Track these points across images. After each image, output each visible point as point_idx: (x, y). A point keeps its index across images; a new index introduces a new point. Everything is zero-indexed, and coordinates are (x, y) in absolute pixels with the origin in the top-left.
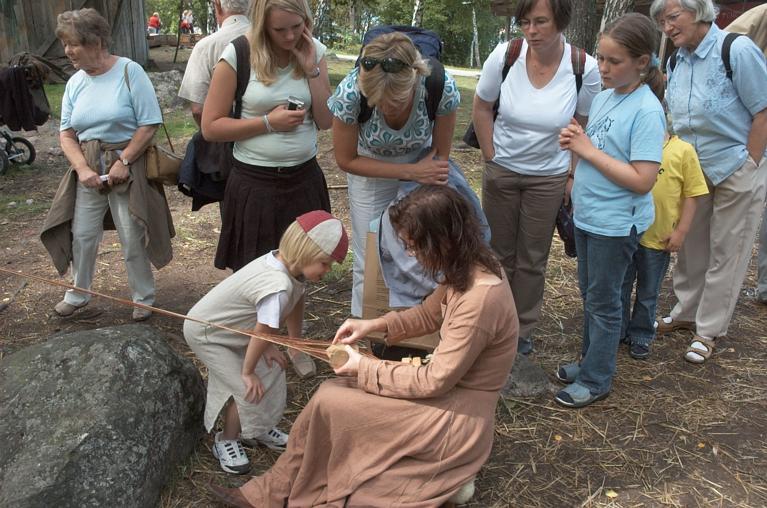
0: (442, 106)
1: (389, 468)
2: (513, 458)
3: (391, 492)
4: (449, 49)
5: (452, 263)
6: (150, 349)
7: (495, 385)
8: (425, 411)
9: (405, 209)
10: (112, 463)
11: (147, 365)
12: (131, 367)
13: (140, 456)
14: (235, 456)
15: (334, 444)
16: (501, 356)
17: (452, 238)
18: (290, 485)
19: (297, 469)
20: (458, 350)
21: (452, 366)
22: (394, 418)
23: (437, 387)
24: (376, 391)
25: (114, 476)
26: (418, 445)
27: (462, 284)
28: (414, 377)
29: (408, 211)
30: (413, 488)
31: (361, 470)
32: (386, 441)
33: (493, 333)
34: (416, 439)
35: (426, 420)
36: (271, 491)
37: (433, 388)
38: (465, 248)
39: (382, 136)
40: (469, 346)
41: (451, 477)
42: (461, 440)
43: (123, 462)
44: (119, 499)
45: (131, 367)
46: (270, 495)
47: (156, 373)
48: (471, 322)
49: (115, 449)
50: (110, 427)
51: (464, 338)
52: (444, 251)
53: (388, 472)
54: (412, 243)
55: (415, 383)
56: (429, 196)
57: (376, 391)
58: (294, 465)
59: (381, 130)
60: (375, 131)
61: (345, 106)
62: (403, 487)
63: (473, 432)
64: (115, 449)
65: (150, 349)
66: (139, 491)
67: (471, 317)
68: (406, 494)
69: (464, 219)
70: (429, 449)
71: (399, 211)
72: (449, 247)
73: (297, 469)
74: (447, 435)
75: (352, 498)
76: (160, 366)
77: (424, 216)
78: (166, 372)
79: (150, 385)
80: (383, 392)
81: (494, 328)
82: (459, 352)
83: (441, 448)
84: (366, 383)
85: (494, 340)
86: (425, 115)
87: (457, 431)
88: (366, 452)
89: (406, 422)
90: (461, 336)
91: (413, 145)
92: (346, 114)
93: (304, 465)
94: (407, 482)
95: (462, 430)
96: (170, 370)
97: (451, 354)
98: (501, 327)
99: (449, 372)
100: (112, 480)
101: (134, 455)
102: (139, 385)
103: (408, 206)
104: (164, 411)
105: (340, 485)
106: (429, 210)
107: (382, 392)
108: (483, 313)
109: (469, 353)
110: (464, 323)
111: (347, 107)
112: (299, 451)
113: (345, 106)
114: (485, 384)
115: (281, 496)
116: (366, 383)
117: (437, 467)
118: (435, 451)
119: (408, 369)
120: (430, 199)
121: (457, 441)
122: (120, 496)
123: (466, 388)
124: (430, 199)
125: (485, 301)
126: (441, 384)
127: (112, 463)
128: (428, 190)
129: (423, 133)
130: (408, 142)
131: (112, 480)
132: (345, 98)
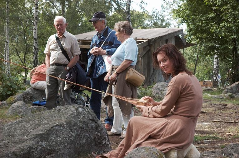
10: (63, 135)
42: (171, 132)
44: (62, 145)
49: (65, 131)
64: (65, 131)
65: (87, 110)
70: (159, 134)
73: (121, 149)
89: (154, 125)
114: (181, 113)
118: (160, 135)
122: (62, 144)
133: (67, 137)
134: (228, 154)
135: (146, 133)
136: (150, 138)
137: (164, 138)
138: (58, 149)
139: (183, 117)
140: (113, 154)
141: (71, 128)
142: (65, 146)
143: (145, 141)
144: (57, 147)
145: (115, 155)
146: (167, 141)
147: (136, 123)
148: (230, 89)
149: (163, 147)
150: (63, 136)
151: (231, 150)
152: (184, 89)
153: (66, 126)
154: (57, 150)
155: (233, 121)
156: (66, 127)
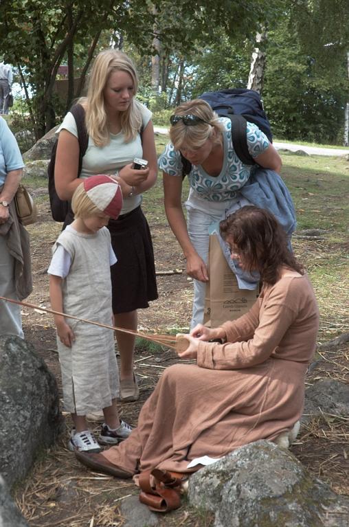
0: (252, 151)
1: (222, 419)
2: (329, 451)
3: (223, 440)
4: (310, 118)
5: (265, 261)
6: (25, 347)
7: (302, 358)
8: (248, 377)
9: (233, 221)
10: (6, 420)
11: (25, 358)
12: (13, 357)
13: (26, 418)
14: (90, 443)
15: (178, 410)
16: (307, 332)
17: (265, 243)
18: (141, 448)
19: (147, 436)
20: (270, 324)
21: (268, 336)
22: (226, 382)
23: (256, 354)
24: (212, 366)
25: (8, 428)
26: (244, 399)
27: (273, 279)
28: (239, 349)
29: (234, 223)
30: (240, 434)
31: (200, 422)
32: (219, 400)
33: (296, 311)
34: (242, 396)
35: (249, 382)
36: (127, 452)
37: (253, 354)
38: (273, 251)
39: (204, 184)
40: (279, 321)
41: (269, 427)
42: (276, 397)
43: (14, 419)
44: (12, 446)
45: (13, 357)
46: (126, 454)
47: (31, 365)
48: (280, 302)
49: (8, 410)
50: (4, 393)
51: (275, 314)
52: (259, 254)
53: (220, 423)
54: (236, 246)
55: (240, 352)
56: (250, 212)
57: (212, 366)
58: (145, 432)
59: (202, 179)
60: (198, 180)
61: (168, 161)
62: (232, 435)
63: (285, 392)
64: (8, 410)
65: (25, 347)
66: (25, 444)
67: (280, 298)
68: (235, 440)
69: (274, 231)
70: (252, 403)
71: (228, 223)
72: (263, 250)
73: (147, 436)
74: (266, 393)
75: (193, 448)
76: (34, 361)
77: (245, 227)
78: (39, 366)
79: (28, 373)
80: (216, 367)
81: (297, 307)
82: (271, 326)
83: (261, 403)
84: (204, 361)
85: (297, 318)
86: (236, 162)
87: (273, 390)
88: (203, 412)
89: (234, 384)
90: (273, 313)
91: (231, 188)
92: (169, 167)
93: (152, 433)
94: (236, 429)
95: (278, 389)
96: (41, 365)
97: (266, 328)
98: (302, 307)
99: (265, 341)
100: (7, 431)
101: (21, 416)
102: (20, 371)
103: (234, 219)
104: (38, 395)
105: (182, 439)
106: (250, 224)
107: (216, 367)
108: (288, 294)
109: (279, 326)
110: (275, 303)
111: (170, 162)
112: (149, 422)
113: (168, 161)
114: (292, 356)
115: (135, 457)
116: (204, 361)
117: (257, 419)
118: (256, 406)
119: (234, 350)
120: (251, 215)
121: (273, 398)
122: (13, 444)
123: (280, 359)
124: (251, 215)
125: (291, 284)
126: (259, 351)
127: (6, 420)
128: (248, 209)
129: (238, 177)
130: (227, 186)
131: (7, 431)
132: (169, 156)
133: (17, 424)
134: (327, 407)
135: (220, 404)
136: (233, 413)
137: (264, 412)
138: (8, 459)
139: (296, 363)
140: (130, 448)
141: (19, 402)
142: (18, 447)
143: (222, 419)
144: (5, 453)
145: (136, 451)
146: (267, 418)
147: (186, 381)
148: (47, 146)
149: (264, 430)
150: (8, 422)
151: (330, 396)
152: (301, 313)
153: (7, 397)
154: (7, 461)
155: (171, 272)
156: (8, 401)
